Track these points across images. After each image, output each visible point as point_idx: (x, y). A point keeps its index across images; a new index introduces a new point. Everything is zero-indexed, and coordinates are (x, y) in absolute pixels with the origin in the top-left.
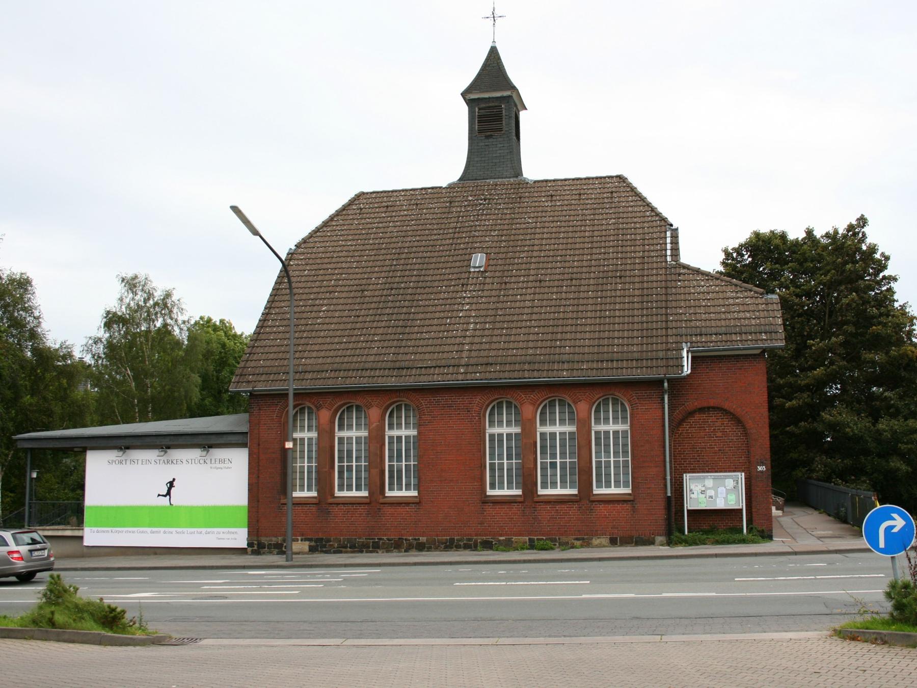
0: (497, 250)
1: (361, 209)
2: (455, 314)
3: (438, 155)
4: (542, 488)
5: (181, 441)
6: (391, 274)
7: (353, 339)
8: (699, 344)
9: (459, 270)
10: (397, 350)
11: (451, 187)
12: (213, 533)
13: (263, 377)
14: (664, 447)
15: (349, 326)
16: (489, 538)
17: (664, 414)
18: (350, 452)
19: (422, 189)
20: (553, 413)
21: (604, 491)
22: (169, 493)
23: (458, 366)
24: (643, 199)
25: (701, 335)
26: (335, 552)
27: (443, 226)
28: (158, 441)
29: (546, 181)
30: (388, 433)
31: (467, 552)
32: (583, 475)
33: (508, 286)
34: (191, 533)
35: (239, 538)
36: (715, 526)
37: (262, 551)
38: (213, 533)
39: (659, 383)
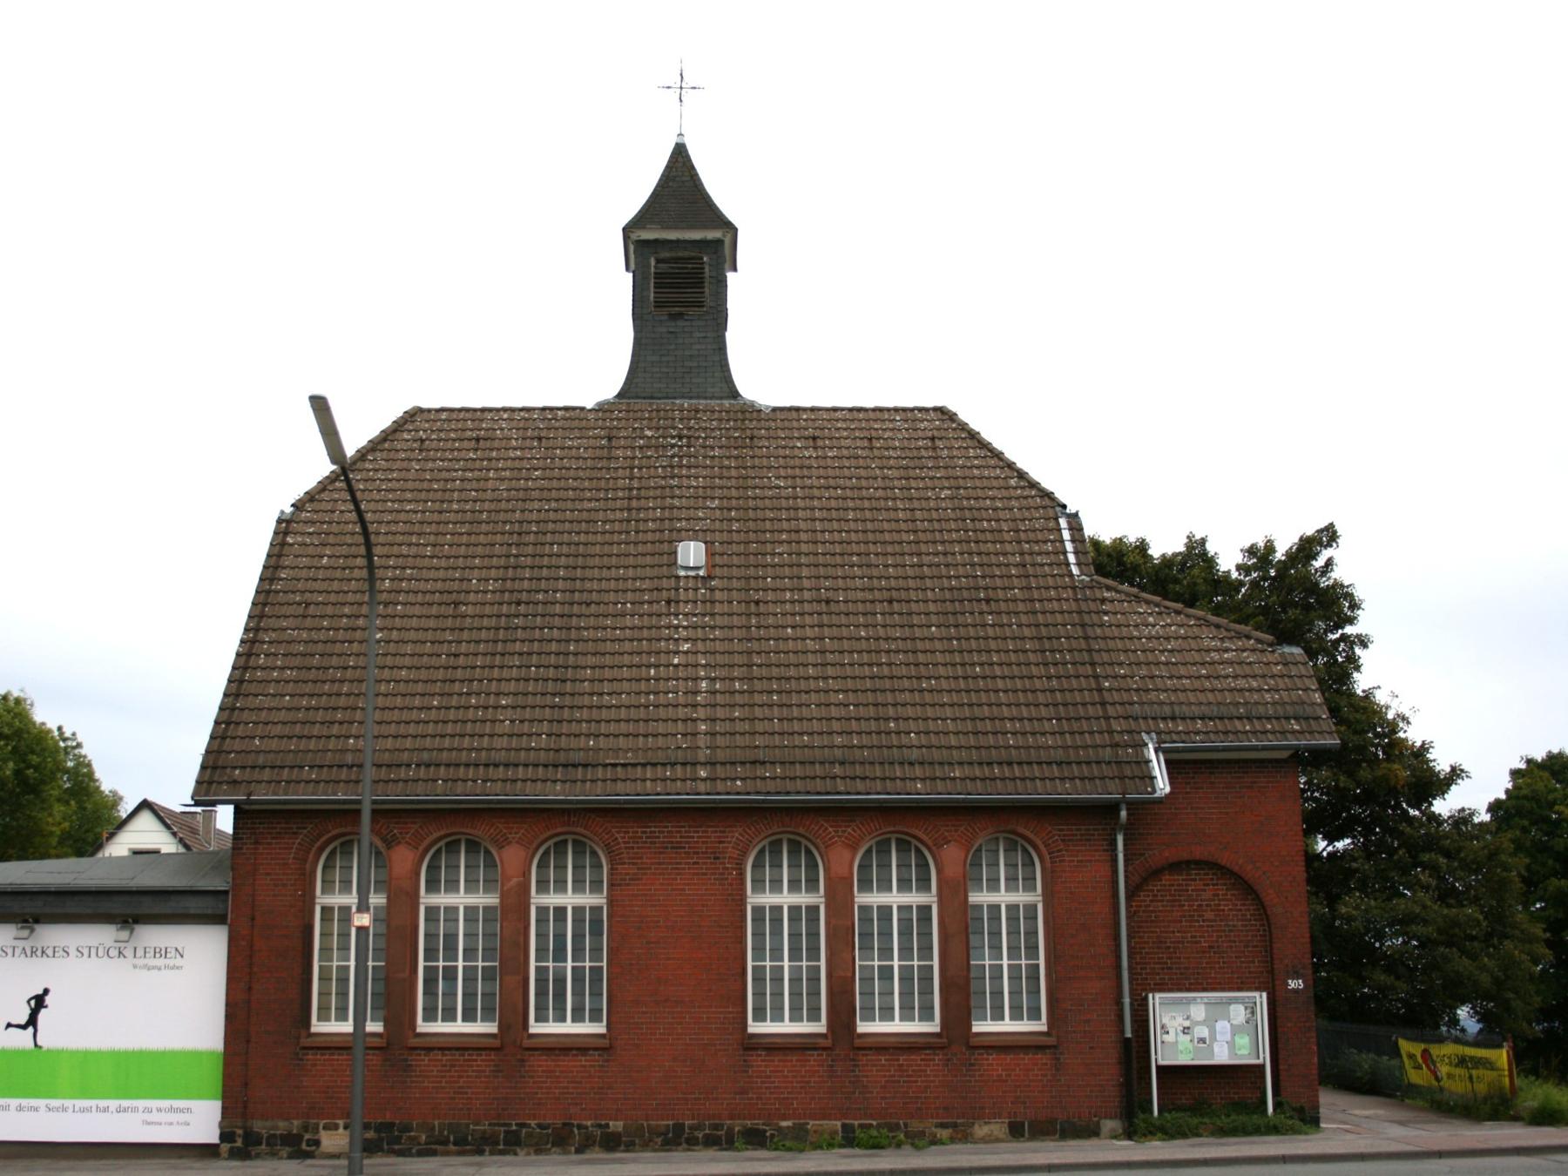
0: (725, 537)
1: (422, 441)
2: (663, 659)
3: (573, 348)
4: (425, 1019)
5: (71, 907)
6: (510, 572)
7: (454, 701)
8: (1175, 737)
9: (656, 572)
10: (555, 728)
11: (603, 408)
12: (135, 1110)
13: (267, 774)
14: (1117, 937)
15: (440, 674)
16: (759, 1123)
17: (1115, 872)
18: (451, 939)
19: (544, 409)
20: (885, 866)
21: (440, 1027)
22: (32, 1021)
23: (694, 764)
24: (998, 455)
25: (1173, 718)
26: (421, 1154)
27: (603, 484)
28: (116, 906)
29: (797, 409)
30: (537, 900)
31: (711, 1153)
32: (508, 995)
33: (762, 608)
34: (83, 1110)
35: (200, 1121)
37: (254, 1150)
38: (135, 1110)
39: (1111, 809)
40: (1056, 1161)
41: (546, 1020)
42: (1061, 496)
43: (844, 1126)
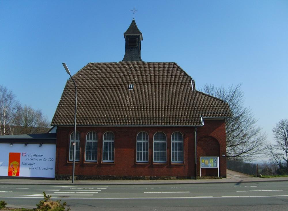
3: (116, 53)
4: (172, 160)
11: (120, 63)
21: (157, 161)
36: (210, 173)
40: (44, 181)
41: (105, 160)
42: (192, 77)
43: (151, 177)
